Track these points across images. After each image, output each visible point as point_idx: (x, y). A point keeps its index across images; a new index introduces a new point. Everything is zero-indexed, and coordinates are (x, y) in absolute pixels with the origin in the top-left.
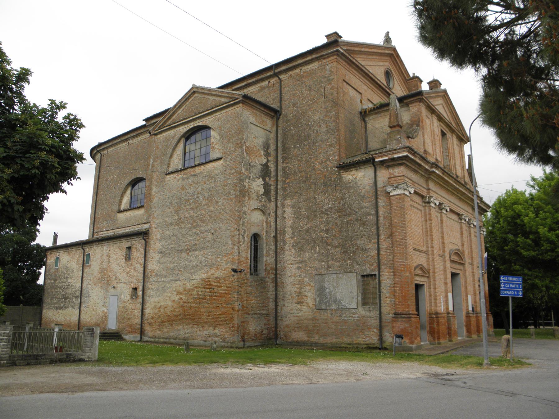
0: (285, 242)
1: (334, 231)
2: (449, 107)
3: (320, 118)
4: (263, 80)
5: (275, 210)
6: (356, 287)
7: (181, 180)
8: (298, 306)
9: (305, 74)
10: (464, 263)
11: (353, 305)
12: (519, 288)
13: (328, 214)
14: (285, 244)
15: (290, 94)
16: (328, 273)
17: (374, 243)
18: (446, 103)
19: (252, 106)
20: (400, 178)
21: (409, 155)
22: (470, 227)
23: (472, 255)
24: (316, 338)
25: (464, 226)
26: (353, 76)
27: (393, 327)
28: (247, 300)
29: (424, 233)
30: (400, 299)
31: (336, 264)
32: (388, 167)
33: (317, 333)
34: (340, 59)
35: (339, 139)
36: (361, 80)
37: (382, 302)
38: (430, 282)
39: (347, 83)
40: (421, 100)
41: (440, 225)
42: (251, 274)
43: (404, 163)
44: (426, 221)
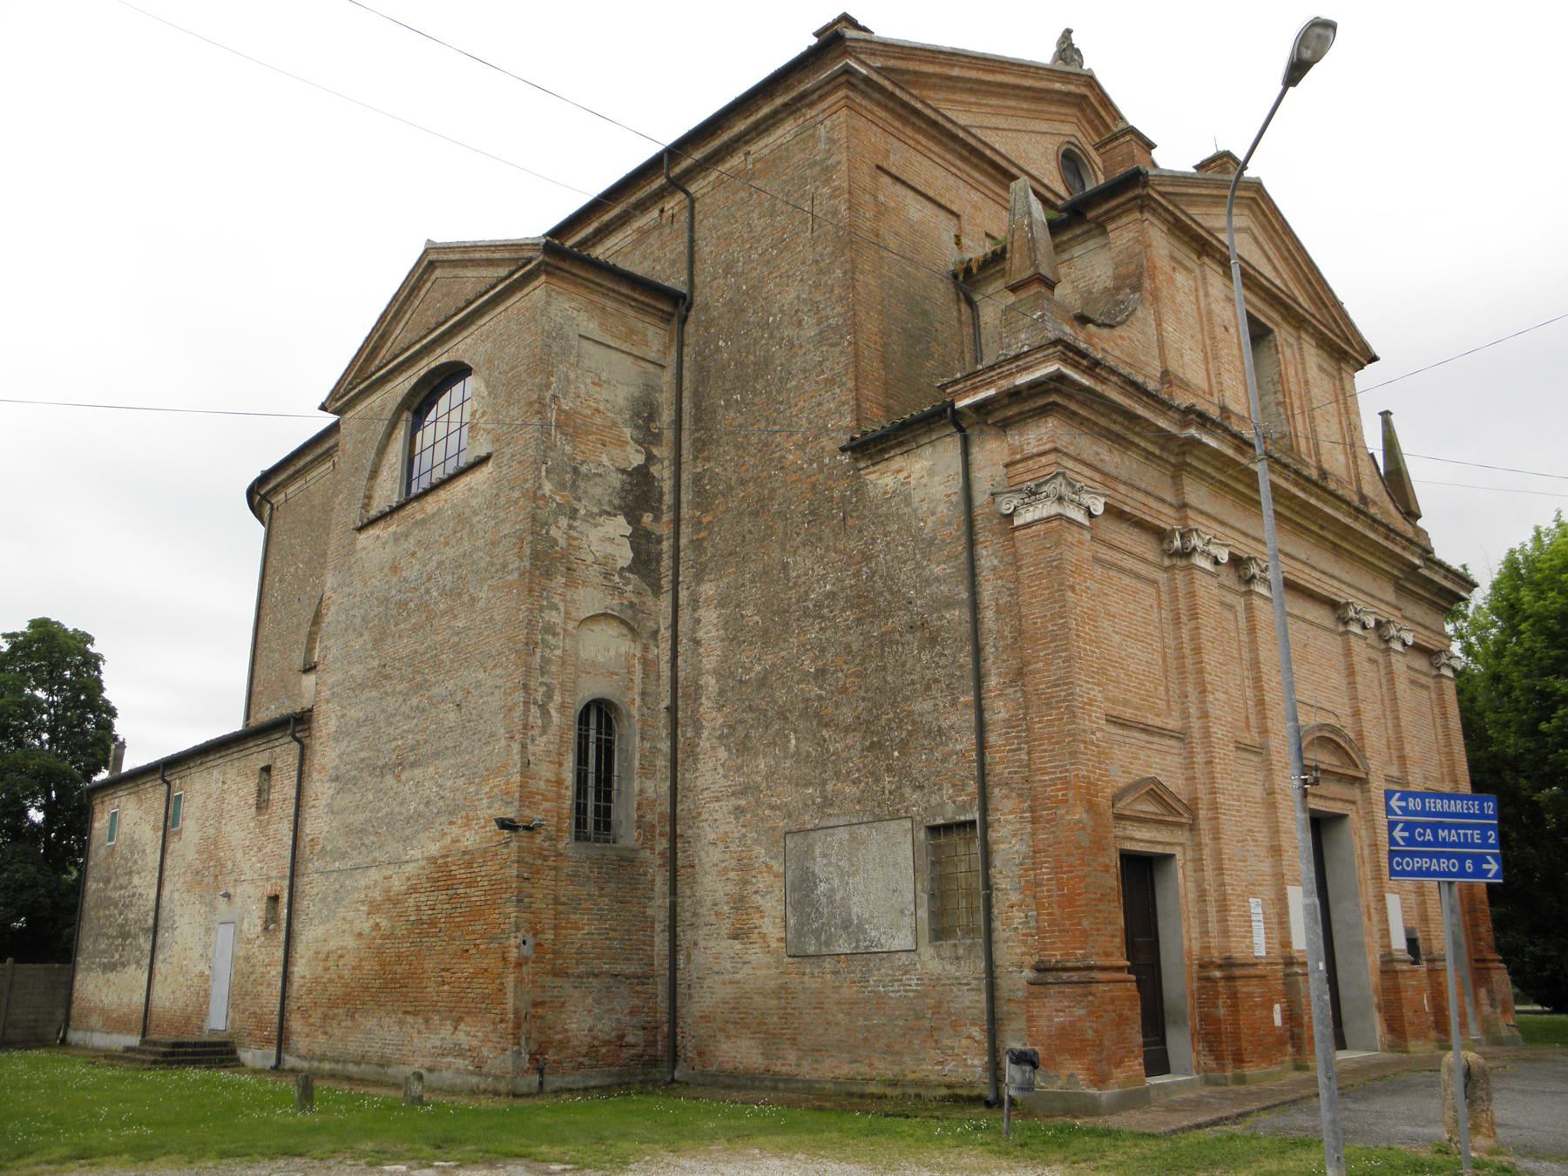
0: (698, 727)
1: (840, 674)
2: (1277, 240)
3: (798, 297)
4: (642, 206)
5: (669, 621)
6: (911, 871)
7: (391, 542)
8: (737, 945)
9: (758, 166)
10: (1364, 776)
11: (903, 940)
12: (1485, 845)
13: (822, 617)
14: (698, 734)
15: (719, 237)
16: (824, 824)
17: (966, 705)
18: (1264, 228)
19: (576, 280)
20: (1043, 460)
21: (1068, 371)
22: (1388, 649)
23: (1401, 749)
24: (789, 1062)
25: (1358, 646)
26: (920, 158)
27: (1030, 1019)
28: (556, 928)
29: (1172, 663)
30: (1056, 911)
31: (847, 790)
32: (1004, 426)
33: (793, 1041)
34: (859, 99)
35: (856, 355)
36: (953, 169)
37: (997, 924)
38: (1199, 846)
39: (897, 179)
40: (1144, 204)
41: (1244, 638)
42: (580, 834)
43: (1054, 404)
44: (1177, 620)
